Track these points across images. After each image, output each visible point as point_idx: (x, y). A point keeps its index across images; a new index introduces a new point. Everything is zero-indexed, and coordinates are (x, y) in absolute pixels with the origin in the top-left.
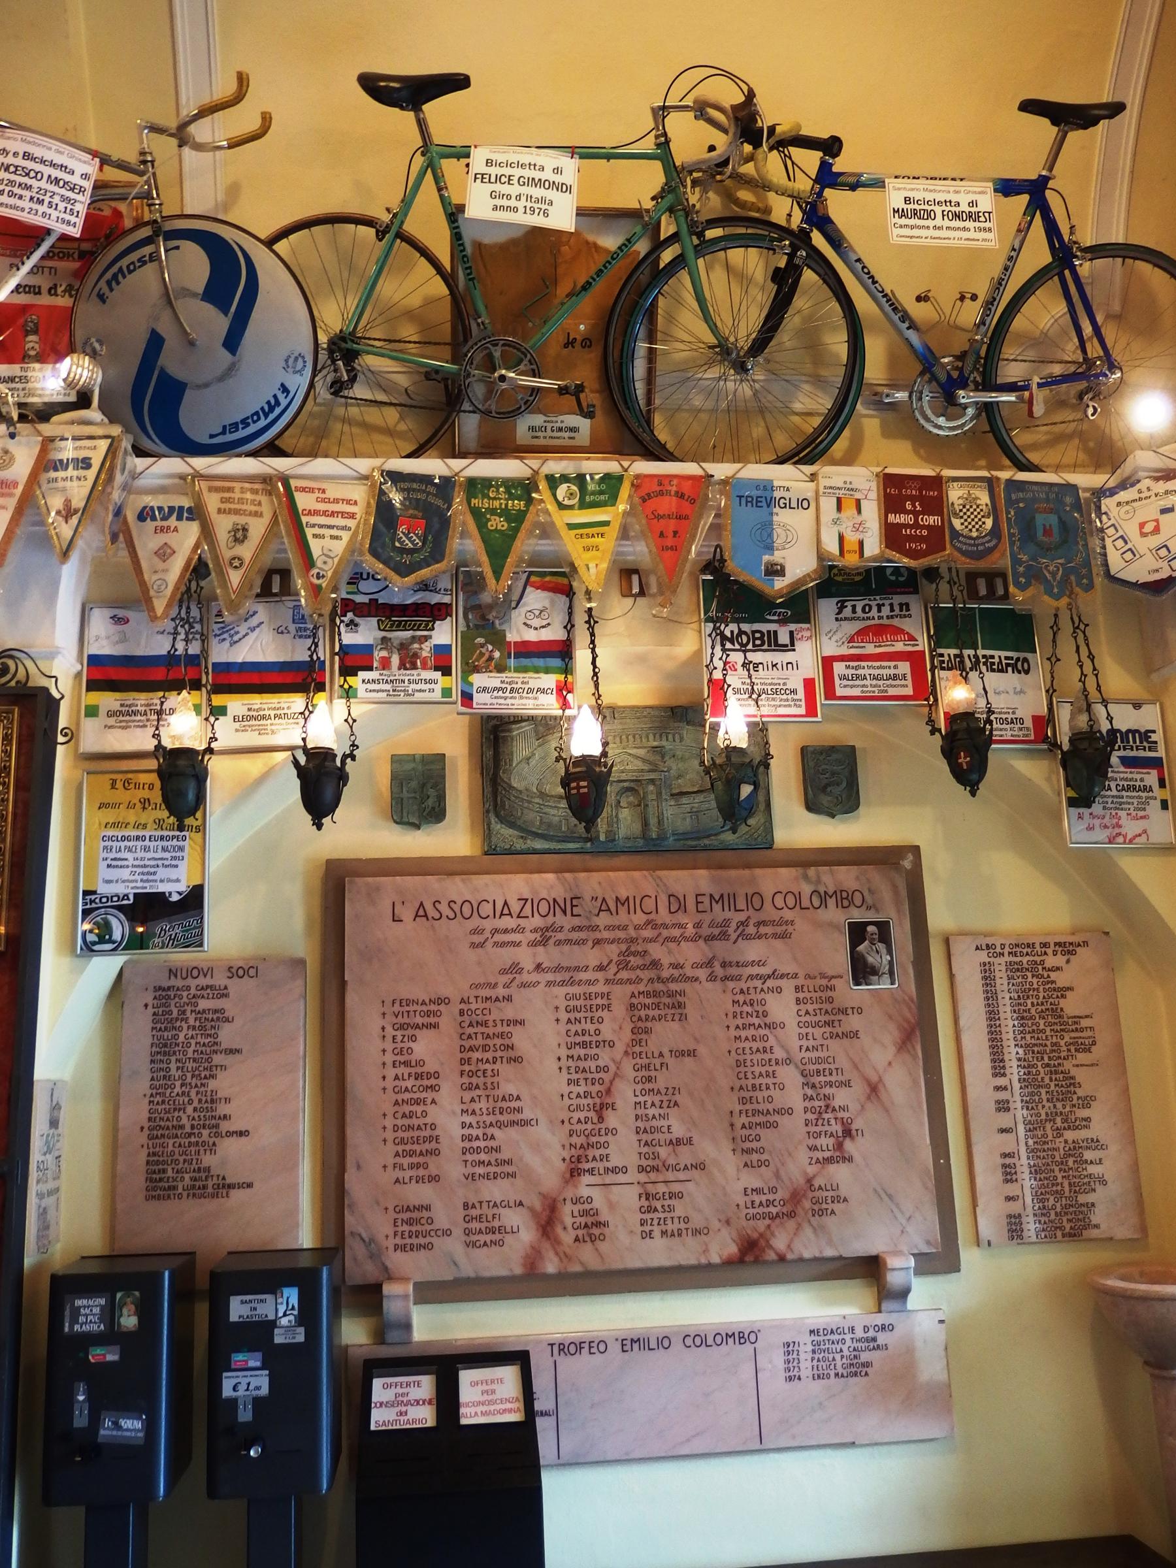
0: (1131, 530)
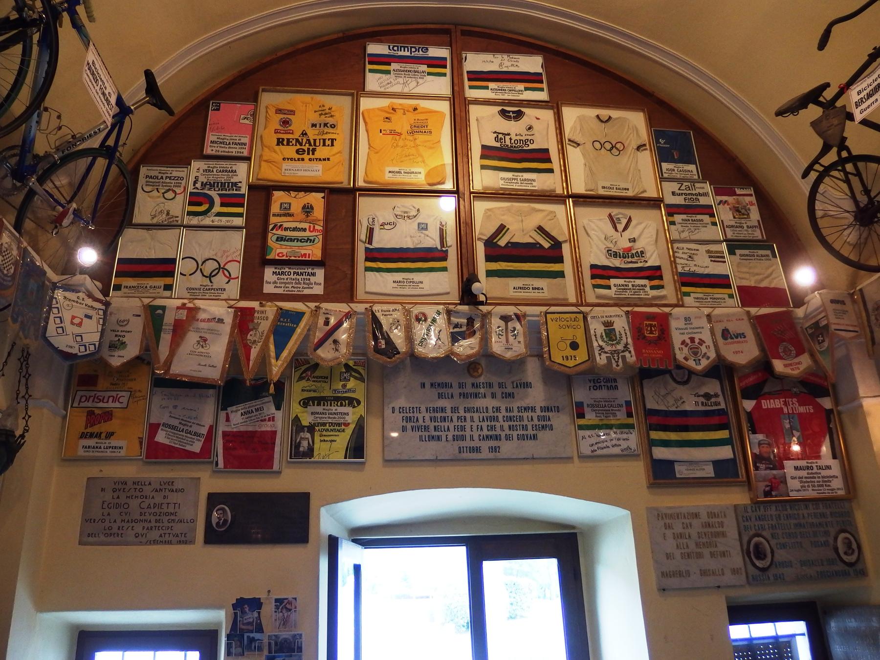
0: (67, 317)
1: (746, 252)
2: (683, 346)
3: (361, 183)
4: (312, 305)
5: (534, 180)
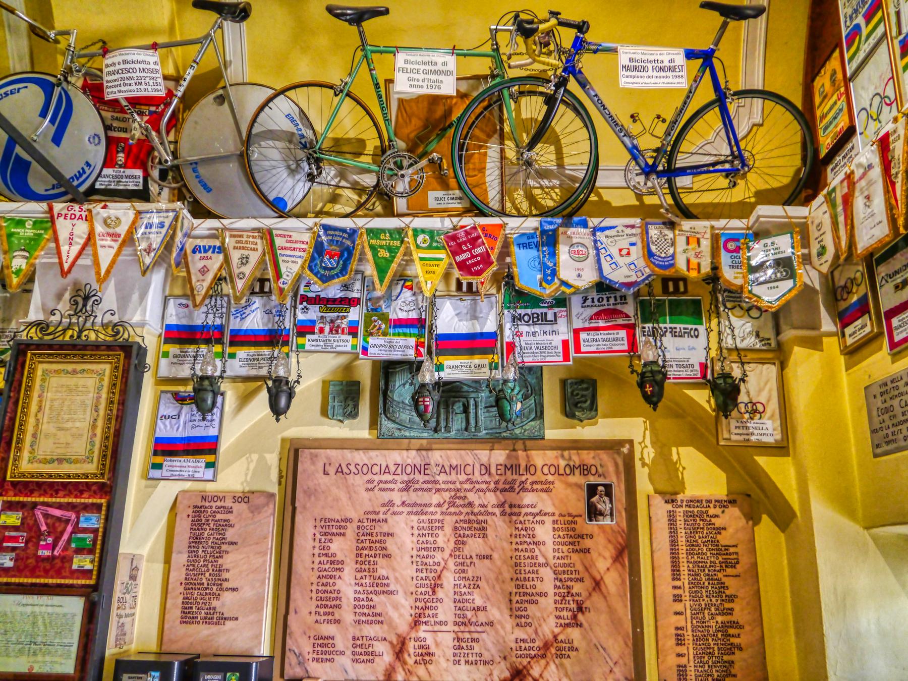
0: (614, 251)
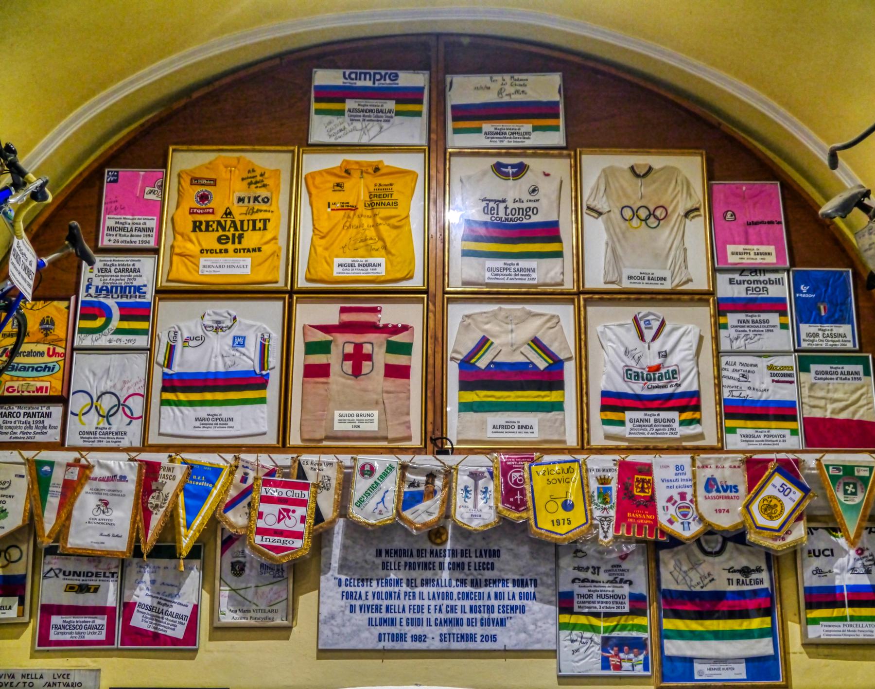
1: (826, 367)
2: (669, 504)
3: (301, 283)
4: (230, 457)
5: (533, 270)
